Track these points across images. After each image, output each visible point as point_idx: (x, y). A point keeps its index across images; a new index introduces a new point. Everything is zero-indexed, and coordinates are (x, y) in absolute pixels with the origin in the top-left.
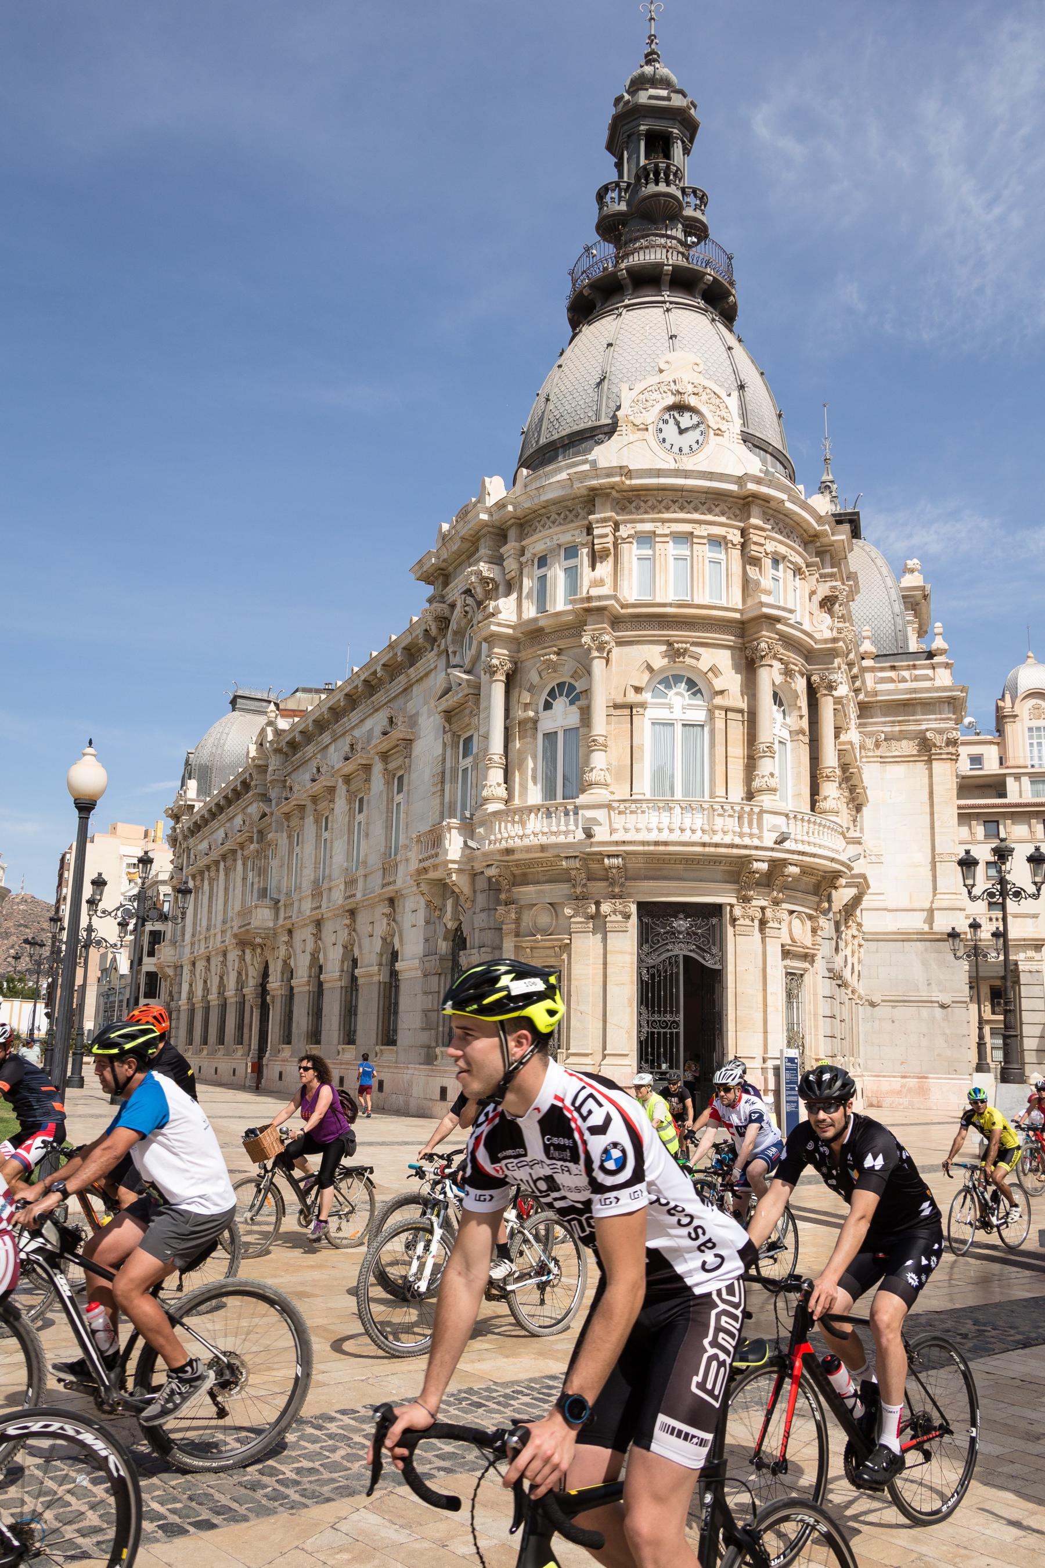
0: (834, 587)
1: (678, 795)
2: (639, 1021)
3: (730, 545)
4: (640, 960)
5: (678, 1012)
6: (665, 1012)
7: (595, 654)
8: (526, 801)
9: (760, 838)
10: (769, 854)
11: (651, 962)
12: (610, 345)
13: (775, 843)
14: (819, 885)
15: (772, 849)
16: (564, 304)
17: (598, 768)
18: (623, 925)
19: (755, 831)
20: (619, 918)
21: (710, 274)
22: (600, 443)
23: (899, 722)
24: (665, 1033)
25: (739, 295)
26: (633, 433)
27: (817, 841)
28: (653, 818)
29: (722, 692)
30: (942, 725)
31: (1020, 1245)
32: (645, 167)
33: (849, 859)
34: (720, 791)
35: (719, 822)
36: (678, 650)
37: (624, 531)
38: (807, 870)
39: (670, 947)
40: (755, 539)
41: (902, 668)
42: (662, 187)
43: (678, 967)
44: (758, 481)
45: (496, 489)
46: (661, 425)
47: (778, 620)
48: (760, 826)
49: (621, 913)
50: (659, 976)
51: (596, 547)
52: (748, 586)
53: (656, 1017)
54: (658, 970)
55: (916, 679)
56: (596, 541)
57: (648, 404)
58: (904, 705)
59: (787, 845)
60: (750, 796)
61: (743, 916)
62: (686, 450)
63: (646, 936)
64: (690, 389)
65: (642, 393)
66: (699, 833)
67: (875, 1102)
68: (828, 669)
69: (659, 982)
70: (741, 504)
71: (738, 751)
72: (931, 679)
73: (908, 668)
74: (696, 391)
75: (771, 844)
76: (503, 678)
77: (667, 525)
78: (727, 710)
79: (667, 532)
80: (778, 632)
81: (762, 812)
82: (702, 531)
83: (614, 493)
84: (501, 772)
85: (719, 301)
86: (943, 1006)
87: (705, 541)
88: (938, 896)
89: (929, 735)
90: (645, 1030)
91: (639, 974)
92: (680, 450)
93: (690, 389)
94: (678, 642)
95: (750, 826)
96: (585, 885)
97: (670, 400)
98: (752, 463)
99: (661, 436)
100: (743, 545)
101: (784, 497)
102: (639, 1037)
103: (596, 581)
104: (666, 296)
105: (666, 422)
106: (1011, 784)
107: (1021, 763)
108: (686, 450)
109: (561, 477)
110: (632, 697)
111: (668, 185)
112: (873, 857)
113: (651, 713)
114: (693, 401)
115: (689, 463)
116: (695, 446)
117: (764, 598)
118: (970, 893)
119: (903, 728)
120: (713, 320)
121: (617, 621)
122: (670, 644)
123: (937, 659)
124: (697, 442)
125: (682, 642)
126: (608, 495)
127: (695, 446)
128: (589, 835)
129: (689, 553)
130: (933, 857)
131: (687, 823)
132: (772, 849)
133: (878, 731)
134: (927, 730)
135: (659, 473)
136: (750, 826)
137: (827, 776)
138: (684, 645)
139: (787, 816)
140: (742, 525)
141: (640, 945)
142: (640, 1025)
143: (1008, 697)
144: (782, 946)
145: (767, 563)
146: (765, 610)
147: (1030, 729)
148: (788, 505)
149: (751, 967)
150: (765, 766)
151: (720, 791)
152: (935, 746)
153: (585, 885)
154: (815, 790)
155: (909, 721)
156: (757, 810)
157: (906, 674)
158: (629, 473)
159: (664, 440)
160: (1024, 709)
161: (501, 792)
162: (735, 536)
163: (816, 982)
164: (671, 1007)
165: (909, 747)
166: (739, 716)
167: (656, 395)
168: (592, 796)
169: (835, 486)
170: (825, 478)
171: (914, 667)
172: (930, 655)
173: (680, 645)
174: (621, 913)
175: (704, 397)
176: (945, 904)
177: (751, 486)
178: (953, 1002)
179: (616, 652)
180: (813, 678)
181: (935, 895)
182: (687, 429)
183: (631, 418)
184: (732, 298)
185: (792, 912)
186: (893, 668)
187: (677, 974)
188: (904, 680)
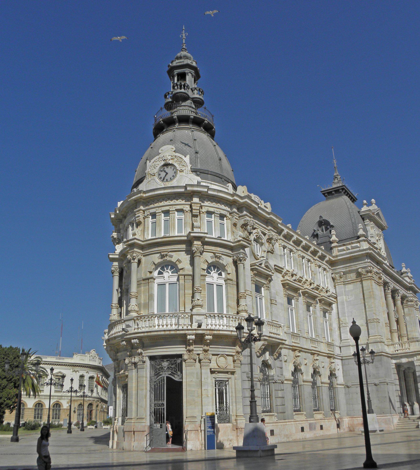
0: (245, 220)
3: (185, 212)
5: (164, 400)
7: (132, 261)
10: (194, 332)
18: (142, 366)
20: (141, 363)
23: (348, 266)
28: (217, 321)
29: (182, 269)
30: (364, 266)
35: (181, 321)
36: (163, 255)
39: (161, 374)
41: (347, 245)
43: (164, 381)
50: (157, 385)
54: (157, 383)
55: (353, 248)
58: (350, 259)
61: (189, 358)
65: (153, 163)
67: (352, 429)
68: (239, 253)
70: (187, 195)
71: (189, 292)
72: (359, 247)
73: (350, 244)
74: (172, 158)
75: (196, 328)
77: (160, 208)
78: (184, 275)
79: (160, 211)
82: (173, 208)
85: (209, 129)
86: (376, 385)
88: (370, 338)
89: (360, 270)
92: (167, 180)
93: (169, 158)
94: (163, 252)
96: (131, 351)
97: (163, 163)
98: (195, 179)
100: (191, 211)
104: (191, 126)
110: (148, 275)
112: (343, 324)
113: (157, 281)
114: (170, 162)
116: (172, 178)
119: (350, 269)
121: (142, 248)
123: (361, 239)
125: (165, 252)
126: (140, 202)
127: (172, 178)
129: (183, 217)
130: (367, 321)
131: (169, 322)
133: (340, 272)
134: (359, 268)
137: (240, 297)
138: (165, 253)
140: (190, 203)
144: (211, 369)
150: (197, 296)
152: (363, 274)
153: (131, 351)
155: (352, 266)
157: (349, 247)
159: (161, 178)
162: (187, 208)
165: (353, 276)
167: (158, 163)
170: (335, 174)
171: (352, 243)
172: (358, 237)
173: (164, 253)
176: (372, 341)
178: (380, 383)
181: (369, 337)
182: (166, 172)
186: (344, 245)
187: (164, 384)
188: (348, 249)
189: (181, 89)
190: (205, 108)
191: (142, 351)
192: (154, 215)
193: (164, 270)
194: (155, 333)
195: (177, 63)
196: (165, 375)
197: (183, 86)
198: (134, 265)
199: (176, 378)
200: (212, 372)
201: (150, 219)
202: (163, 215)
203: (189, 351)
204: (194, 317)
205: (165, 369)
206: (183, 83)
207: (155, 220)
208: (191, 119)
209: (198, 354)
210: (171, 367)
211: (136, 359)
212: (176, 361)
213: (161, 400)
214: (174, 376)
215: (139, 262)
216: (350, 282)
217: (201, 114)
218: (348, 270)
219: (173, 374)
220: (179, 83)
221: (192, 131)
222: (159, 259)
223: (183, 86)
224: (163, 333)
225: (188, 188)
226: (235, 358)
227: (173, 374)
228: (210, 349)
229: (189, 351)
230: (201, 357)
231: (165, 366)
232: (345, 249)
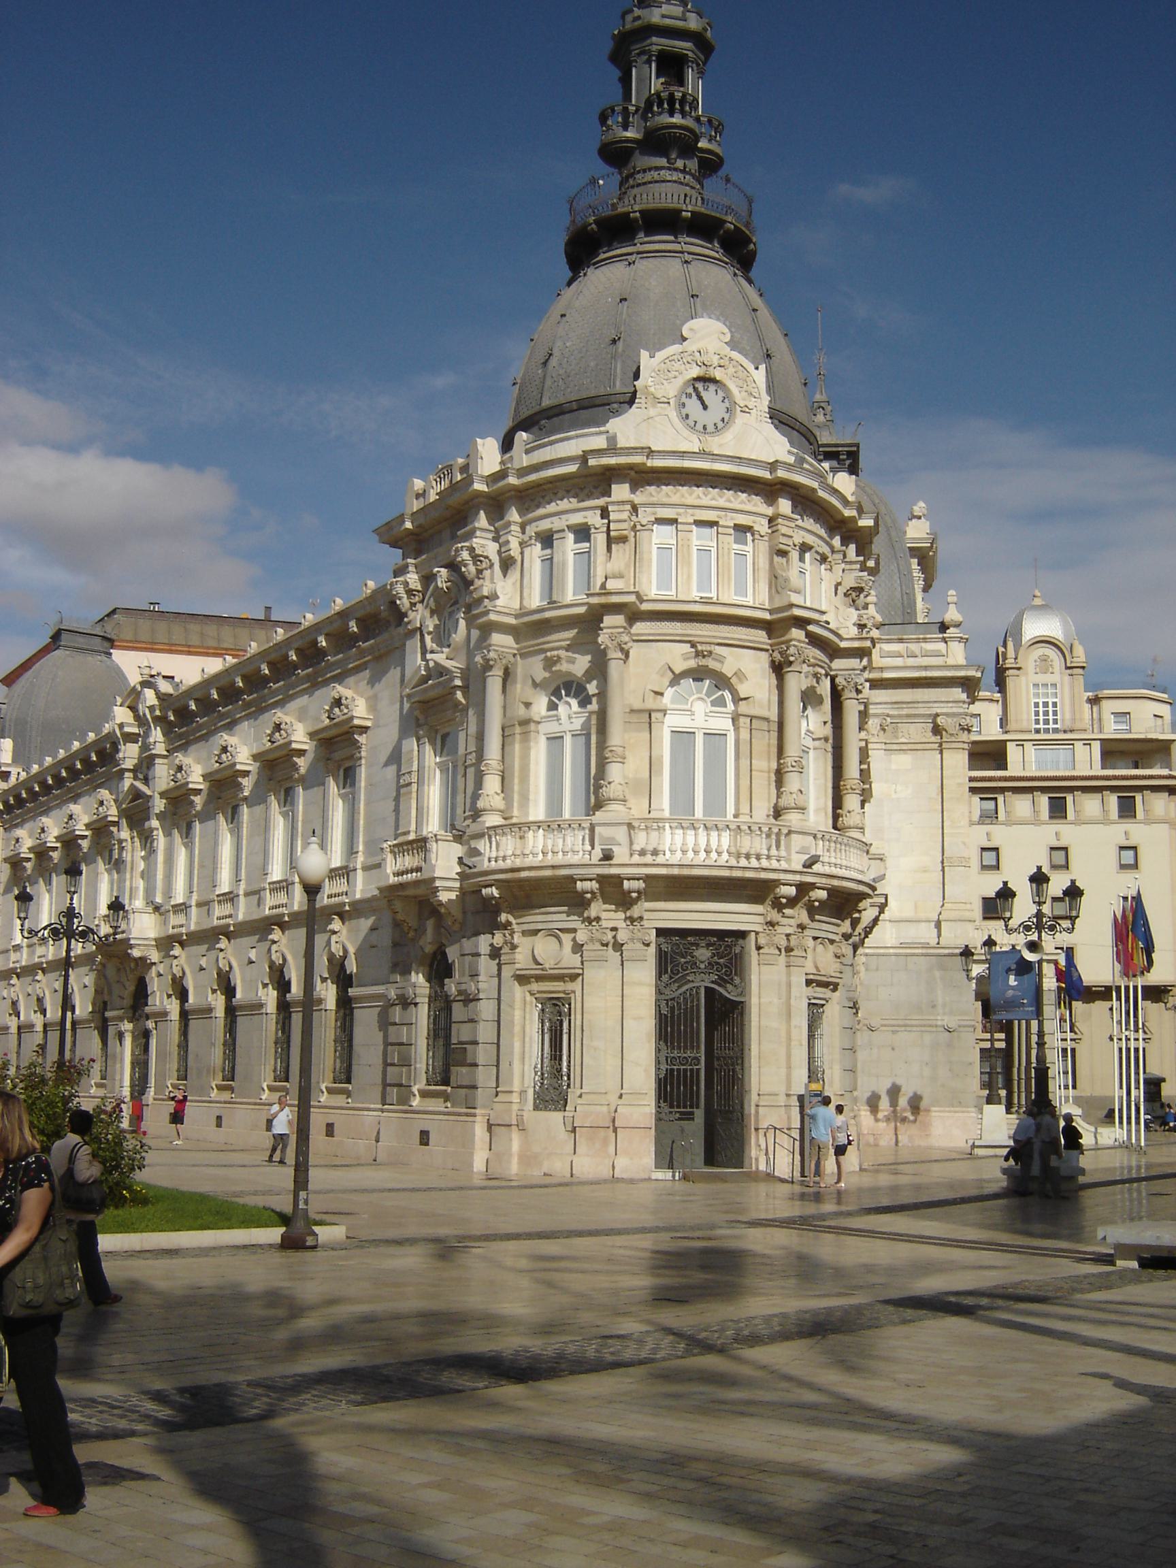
1: (699, 813)
2: (657, 1059)
4: (659, 992)
5: (698, 1047)
6: (686, 1048)
8: (527, 814)
9: (788, 860)
11: (669, 993)
12: (623, 300)
13: (804, 866)
14: (844, 903)
15: (801, 873)
16: (563, 238)
17: (617, 781)
19: (783, 853)
21: (731, 222)
22: (616, 413)
24: (692, 1070)
25: (761, 241)
26: (654, 406)
27: (844, 863)
31: (154, 1433)
32: (658, 94)
33: (874, 880)
34: (745, 808)
37: (644, 516)
38: (833, 892)
40: (784, 530)
42: (677, 119)
44: (789, 467)
45: (489, 456)
46: (684, 399)
47: (808, 621)
48: (788, 848)
49: (639, 940)
51: (612, 533)
52: (777, 582)
53: (676, 1054)
56: (612, 526)
57: (670, 375)
59: (817, 868)
60: (777, 813)
61: (632, 940)
62: (710, 428)
63: (665, 964)
64: (715, 360)
66: (725, 856)
69: (679, 1017)
73: (918, 640)
75: (799, 868)
76: (501, 673)
78: (752, 718)
80: (809, 635)
81: (790, 832)
83: (633, 473)
84: (498, 779)
85: (739, 251)
87: (732, 531)
90: (664, 1067)
91: (658, 1006)
92: (705, 427)
95: (778, 847)
97: (695, 372)
99: (684, 412)
101: (815, 485)
102: (657, 1075)
103: (611, 569)
105: (689, 396)
106: (1012, 752)
107: (1024, 726)
108: (710, 428)
109: (570, 447)
110: (650, 703)
111: (684, 116)
114: (718, 374)
115: (717, 444)
116: (720, 425)
117: (795, 599)
118: (1006, 926)
120: (735, 275)
121: (634, 615)
122: (693, 645)
124: (723, 420)
127: (720, 425)
128: (607, 856)
132: (801, 873)
135: (682, 454)
136: (778, 847)
139: (815, 837)
141: (659, 975)
142: (658, 1062)
143: (1010, 644)
145: (794, 555)
146: (797, 612)
147: (1036, 685)
148: (821, 493)
149: (772, 996)
150: (793, 782)
151: (745, 808)
154: (838, 803)
156: (785, 831)
157: (914, 647)
158: (650, 453)
159: (687, 416)
160: (1030, 659)
161: (498, 802)
163: (834, 1013)
164: (692, 1042)
165: (920, 732)
166: (765, 725)
168: (610, 814)
169: (830, 408)
171: (925, 640)
172: (943, 627)
174: (639, 940)
175: (731, 370)
176: (953, 915)
177: (781, 474)
179: (635, 651)
180: (837, 680)
183: (652, 389)
184: (752, 246)
185: (815, 938)
186: (901, 640)
189: (672, 115)
190: (728, 180)
191: (511, 918)
192: (547, 540)
193: (560, 698)
194: (532, 874)
195: (664, 16)
196: (703, 981)
197: (677, 106)
198: (494, 684)
199: (730, 993)
200: (809, 983)
201: (536, 550)
202: (571, 537)
203: (632, 920)
204: (597, 829)
205: (702, 966)
206: (678, 95)
207: (587, 545)
208: (686, 219)
209: (614, 929)
210: (718, 963)
211: (498, 939)
212: (728, 944)
213: (692, 1048)
214: (725, 988)
215: (507, 674)
216: (904, 747)
217: (713, 198)
218: (905, 712)
219: (722, 982)
220: (664, 95)
221: (686, 262)
222: (686, 659)
223: (677, 106)
224: (548, 873)
225: (592, 462)
226: (793, 943)
227: (722, 982)
228: (784, 921)
229: (632, 920)
230: (622, 936)
231: (703, 958)
232: (918, 653)
